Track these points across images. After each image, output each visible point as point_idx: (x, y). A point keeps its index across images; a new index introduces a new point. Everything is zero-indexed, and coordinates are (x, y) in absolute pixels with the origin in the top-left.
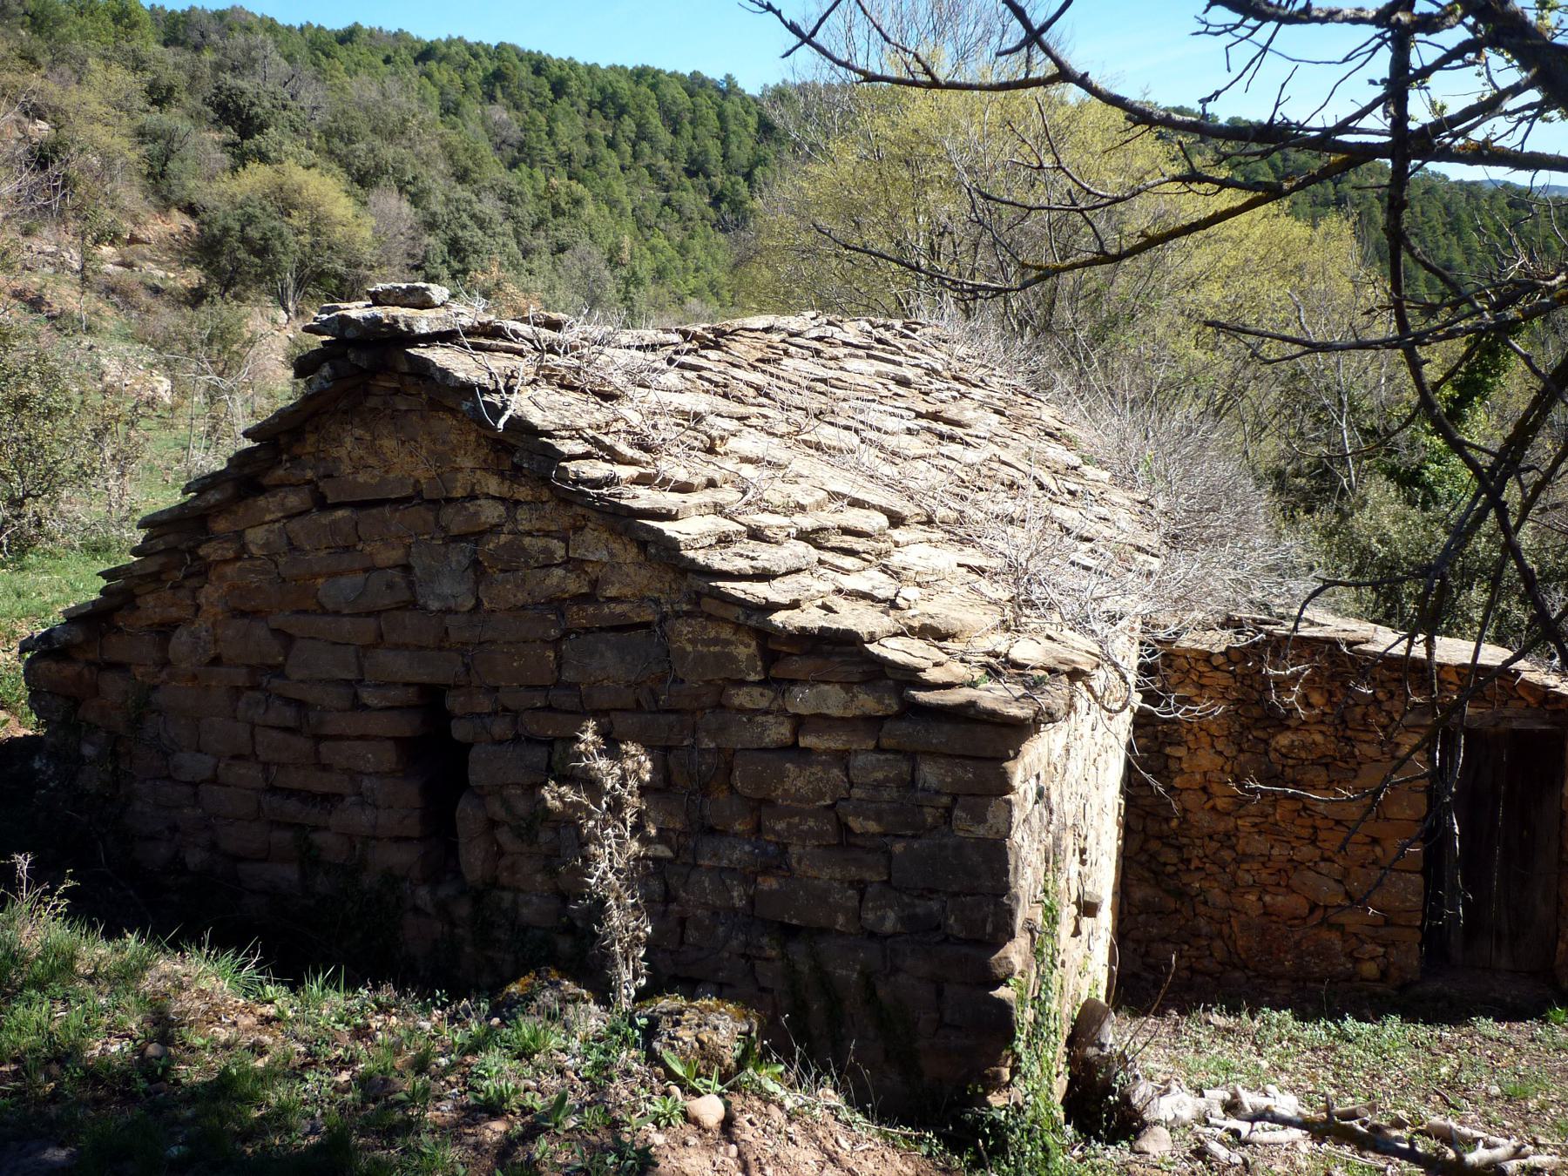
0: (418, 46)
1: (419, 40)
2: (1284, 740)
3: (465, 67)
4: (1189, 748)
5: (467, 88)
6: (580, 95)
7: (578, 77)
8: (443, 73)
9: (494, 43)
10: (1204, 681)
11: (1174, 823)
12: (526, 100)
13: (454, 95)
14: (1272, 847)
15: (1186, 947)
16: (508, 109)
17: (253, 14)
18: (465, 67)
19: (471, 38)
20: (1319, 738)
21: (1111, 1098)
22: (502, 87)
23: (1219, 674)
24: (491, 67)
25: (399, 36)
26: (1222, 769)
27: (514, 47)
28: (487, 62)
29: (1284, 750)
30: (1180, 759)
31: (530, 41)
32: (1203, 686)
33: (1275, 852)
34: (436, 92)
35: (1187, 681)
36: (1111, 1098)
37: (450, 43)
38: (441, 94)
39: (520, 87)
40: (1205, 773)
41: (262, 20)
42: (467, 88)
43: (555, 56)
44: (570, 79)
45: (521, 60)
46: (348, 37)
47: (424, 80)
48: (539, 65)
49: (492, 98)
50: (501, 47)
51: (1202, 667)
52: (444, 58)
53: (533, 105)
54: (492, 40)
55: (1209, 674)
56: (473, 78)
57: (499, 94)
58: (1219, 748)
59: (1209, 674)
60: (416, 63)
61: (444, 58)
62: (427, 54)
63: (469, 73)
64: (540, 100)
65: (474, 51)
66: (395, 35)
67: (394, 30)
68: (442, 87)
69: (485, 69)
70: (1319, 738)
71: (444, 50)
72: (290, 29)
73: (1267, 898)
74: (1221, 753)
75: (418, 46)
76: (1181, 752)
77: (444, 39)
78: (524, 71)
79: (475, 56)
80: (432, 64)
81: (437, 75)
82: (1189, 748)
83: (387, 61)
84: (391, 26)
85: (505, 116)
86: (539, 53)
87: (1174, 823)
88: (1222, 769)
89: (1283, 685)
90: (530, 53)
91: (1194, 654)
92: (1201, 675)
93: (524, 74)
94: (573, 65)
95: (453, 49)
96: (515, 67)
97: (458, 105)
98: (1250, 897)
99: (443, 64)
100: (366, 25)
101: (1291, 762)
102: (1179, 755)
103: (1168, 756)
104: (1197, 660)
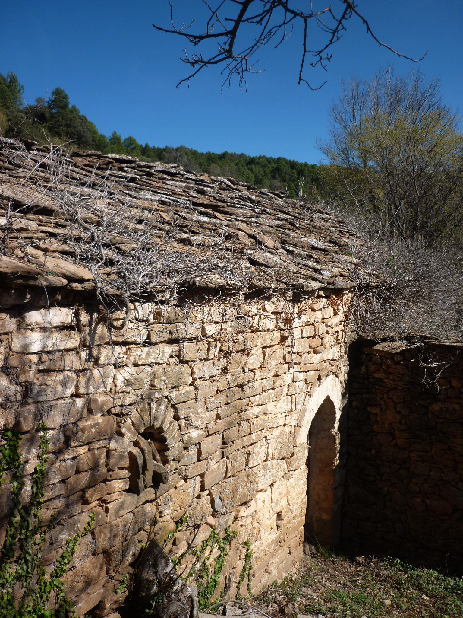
0: (248, 159)
1: (249, 157)
2: (436, 407)
3: (265, 166)
4: (382, 409)
5: (265, 174)
6: (308, 176)
7: (308, 170)
8: (256, 169)
9: (277, 157)
10: (390, 370)
11: (373, 452)
12: (288, 178)
13: (260, 176)
14: (430, 471)
15: (379, 525)
16: (280, 182)
17: (188, 149)
18: (265, 166)
19: (268, 156)
20: (456, 407)
21: (147, 611)
22: (279, 174)
23: (398, 366)
24: (274, 166)
25: (242, 156)
26: (400, 422)
27: (285, 160)
28: (273, 164)
29: (436, 413)
30: (376, 414)
31: (290, 157)
32: (390, 373)
33: (432, 473)
34: (253, 175)
35: (381, 370)
36: (147, 611)
37: (260, 157)
38: (256, 176)
39: (285, 173)
40: (391, 423)
41: (191, 151)
42: (265, 174)
43: (300, 161)
44: (305, 170)
45: (286, 163)
46: (223, 156)
47: (249, 171)
48: (293, 165)
49: (274, 178)
50: (279, 159)
51: (389, 362)
52: (258, 163)
53: (290, 180)
54: (276, 156)
55: (393, 366)
56: (268, 170)
57: (277, 176)
58: (398, 409)
59: (393, 366)
60: (247, 165)
61: (258, 163)
62: (251, 162)
63: (266, 169)
64: (293, 178)
65: (269, 160)
66: (240, 155)
67: (240, 153)
68: (256, 174)
69: (273, 167)
70: (456, 407)
71: (258, 160)
72: (202, 154)
73: (428, 501)
74: (399, 413)
75: (248, 159)
76: (377, 410)
77: (258, 156)
78: (288, 168)
79: (269, 162)
80: (253, 166)
81: (254, 169)
82: (382, 409)
83: (237, 164)
84: (239, 152)
85: (279, 184)
86: (294, 161)
87: (373, 452)
88: (400, 422)
89: (431, 373)
90: (290, 161)
91: (384, 354)
92: (388, 366)
93: (287, 169)
94: (306, 165)
95: (261, 160)
96: (284, 166)
97: (261, 180)
98: (417, 500)
99: (257, 165)
100: (230, 152)
101: (440, 420)
102: (375, 412)
103: (370, 413)
104: (387, 358)
